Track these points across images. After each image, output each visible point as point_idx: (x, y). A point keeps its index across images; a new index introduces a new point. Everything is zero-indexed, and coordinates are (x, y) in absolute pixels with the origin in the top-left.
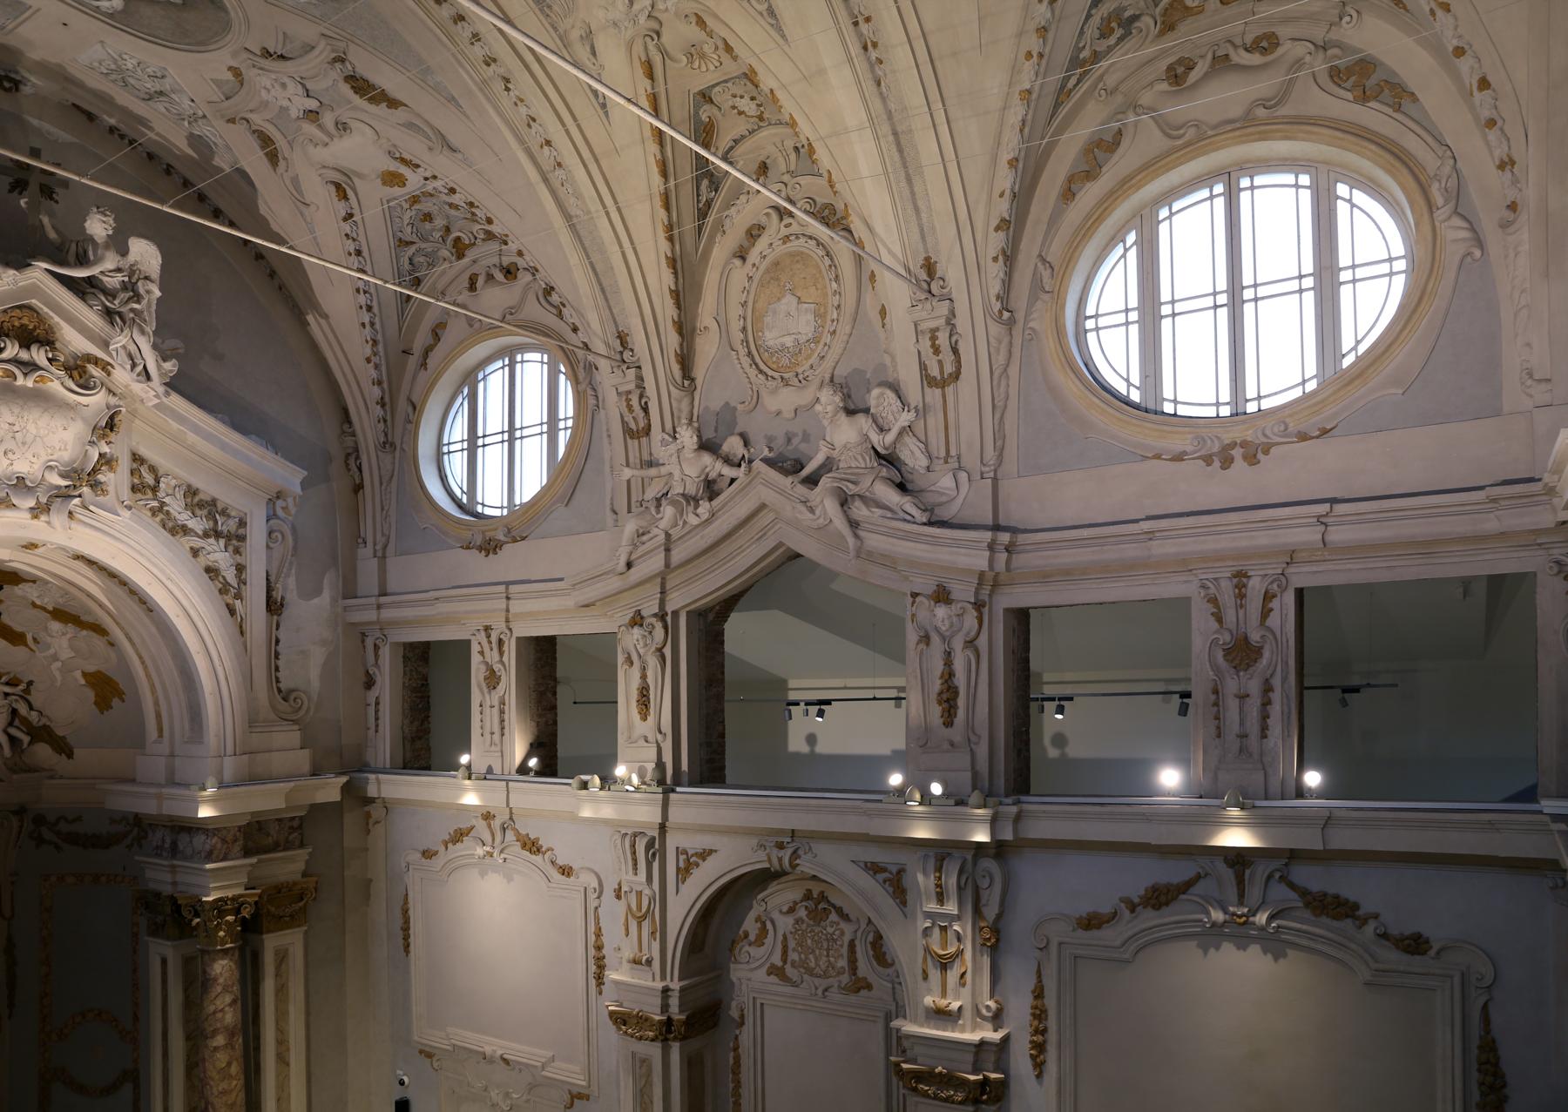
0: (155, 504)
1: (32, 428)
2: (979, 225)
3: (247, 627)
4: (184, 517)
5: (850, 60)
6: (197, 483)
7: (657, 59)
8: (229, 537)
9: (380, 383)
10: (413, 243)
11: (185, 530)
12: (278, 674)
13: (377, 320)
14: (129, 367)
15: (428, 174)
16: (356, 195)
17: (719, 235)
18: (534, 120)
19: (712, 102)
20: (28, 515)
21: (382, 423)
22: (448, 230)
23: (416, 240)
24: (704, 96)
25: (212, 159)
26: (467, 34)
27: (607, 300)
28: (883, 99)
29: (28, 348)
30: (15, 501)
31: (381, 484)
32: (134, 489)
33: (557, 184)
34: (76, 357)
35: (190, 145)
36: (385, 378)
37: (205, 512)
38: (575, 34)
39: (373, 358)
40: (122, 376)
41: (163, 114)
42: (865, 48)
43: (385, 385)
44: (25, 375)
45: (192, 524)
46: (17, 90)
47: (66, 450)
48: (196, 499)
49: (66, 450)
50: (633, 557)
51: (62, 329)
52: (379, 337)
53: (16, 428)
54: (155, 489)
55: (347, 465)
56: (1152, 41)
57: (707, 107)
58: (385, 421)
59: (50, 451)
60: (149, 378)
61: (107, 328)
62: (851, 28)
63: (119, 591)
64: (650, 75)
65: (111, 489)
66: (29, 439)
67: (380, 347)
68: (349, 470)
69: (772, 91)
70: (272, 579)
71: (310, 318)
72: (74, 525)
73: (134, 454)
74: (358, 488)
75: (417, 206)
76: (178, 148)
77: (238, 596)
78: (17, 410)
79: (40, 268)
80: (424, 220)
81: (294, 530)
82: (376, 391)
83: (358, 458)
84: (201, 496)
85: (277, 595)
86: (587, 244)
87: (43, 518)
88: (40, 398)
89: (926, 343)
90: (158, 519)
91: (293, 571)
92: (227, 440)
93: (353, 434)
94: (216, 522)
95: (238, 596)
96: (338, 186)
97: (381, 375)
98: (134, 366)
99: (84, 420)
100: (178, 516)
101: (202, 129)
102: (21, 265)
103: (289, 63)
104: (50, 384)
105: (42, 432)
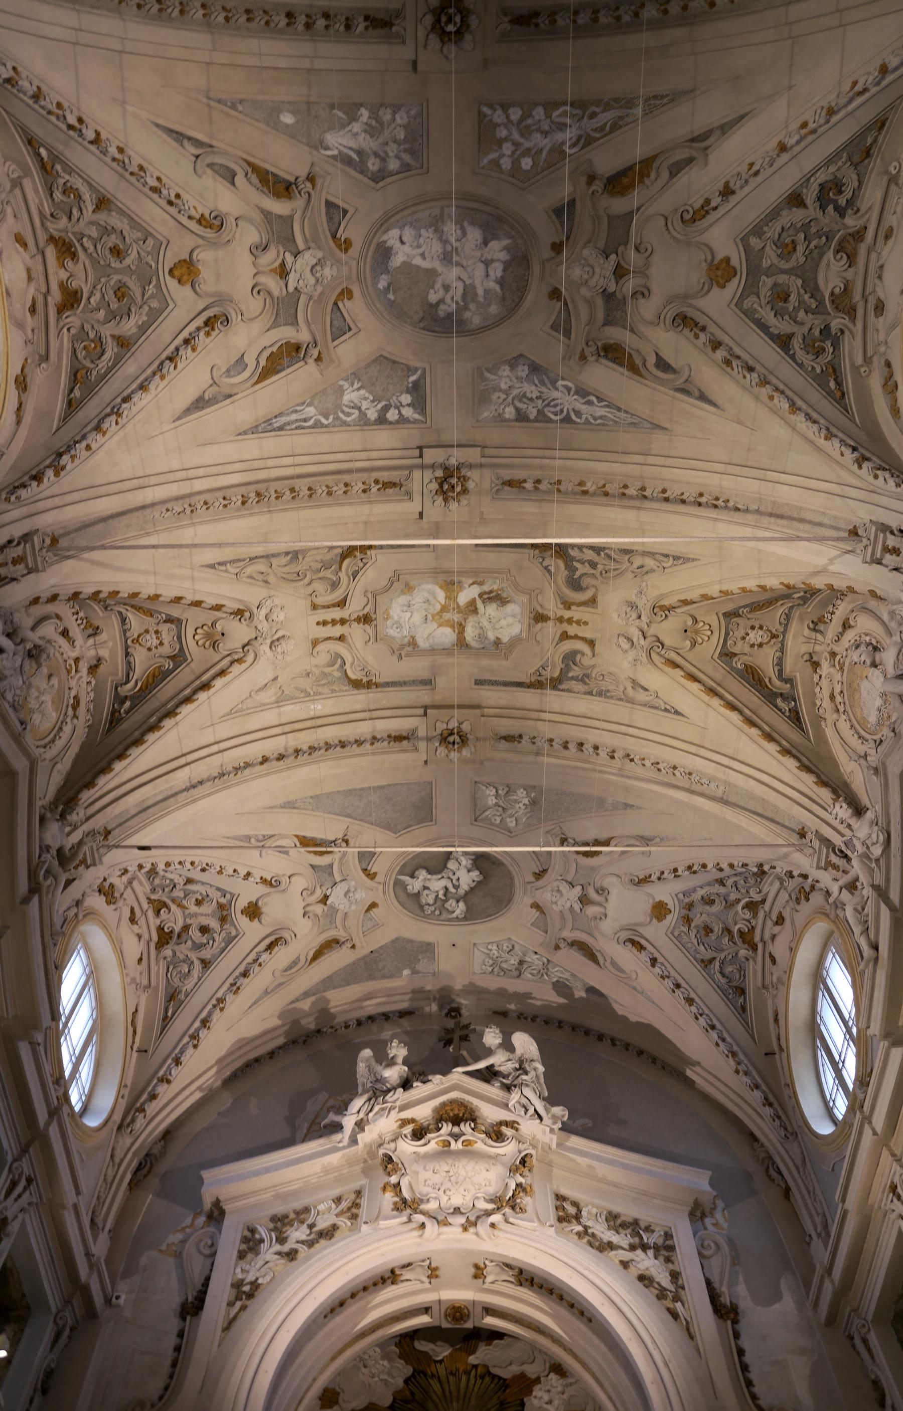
0: (579, 1228)
1: (462, 1172)
2: (851, 480)
3: (695, 1330)
4: (609, 1236)
5: (716, 520)
6: (616, 1208)
7: (673, 656)
8: (657, 1248)
9: (757, 1087)
10: (714, 959)
11: (611, 1246)
12: (752, 1389)
13: (725, 1035)
14: (523, 1113)
15: (658, 874)
16: (648, 940)
17: (823, 724)
18: (658, 763)
19: (735, 655)
20: (461, 1229)
21: (777, 1120)
22: (729, 931)
23: (713, 955)
24: (727, 655)
25: (573, 994)
26: (591, 750)
27: (778, 823)
28: (747, 511)
29: (459, 1126)
30: (450, 1220)
31: (799, 1172)
32: (560, 1220)
33: (698, 788)
34: (492, 1126)
35: (559, 994)
36: (759, 1081)
37: (629, 1231)
38: (630, 691)
39: (740, 1068)
40: (529, 1127)
41: (533, 981)
42: (716, 506)
43: (764, 1087)
44: (456, 1141)
45: (615, 1238)
46: (460, 1015)
47: (490, 1185)
48: (619, 1222)
49: (490, 1185)
50: (872, 937)
51: (472, 1103)
52: (735, 1048)
53: (451, 1174)
54: (578, 1217)
55: (769, 1176)
56: (854, 324)
57: (736, 659)
58: (779, 1118)
59: (477, 1187)
60: (540, 1118)
61: (505, 1094)
62: (701, 509)
63: (564, 1312)
64: (676, 665)
65: (529, 1208)
66: (461, 1179)
67: (742, 1057)
68: (773, 1180)
69: (721, 592)
70: (716, 1285)
71: (689, 1073)
72: (496, 1232)
73: (557, 1195)
74: (787, 1192)
75: (693, 925)
76: (555, 1002)
77: (677, 1298)
78: (450, 1162)
79: (458, 1072)
80: (707, 935)
81: (731, 1242)
82: (757, 1094)
83: (774, 1163)
84: (623, 1218)
85: (726, 1300)
86: (742, 803)
87: (472, 1230)
88: (468, 1153)
89: (889, 559)
90: (585, 1240)
91: (741, 1279)
92: (628, 1162)
93: (762, 1146)
94: (642, 1238)
95: (677, 1298)
96: (633, 942)
97: (754, 1078)
98: (526, 1110)
99: (503, 1164)
100: (602, 1236)
101: (556, 974)
102: (445, 1072)
103: (549, 871)
104: (476, 1145)
105: (470, 1174)
